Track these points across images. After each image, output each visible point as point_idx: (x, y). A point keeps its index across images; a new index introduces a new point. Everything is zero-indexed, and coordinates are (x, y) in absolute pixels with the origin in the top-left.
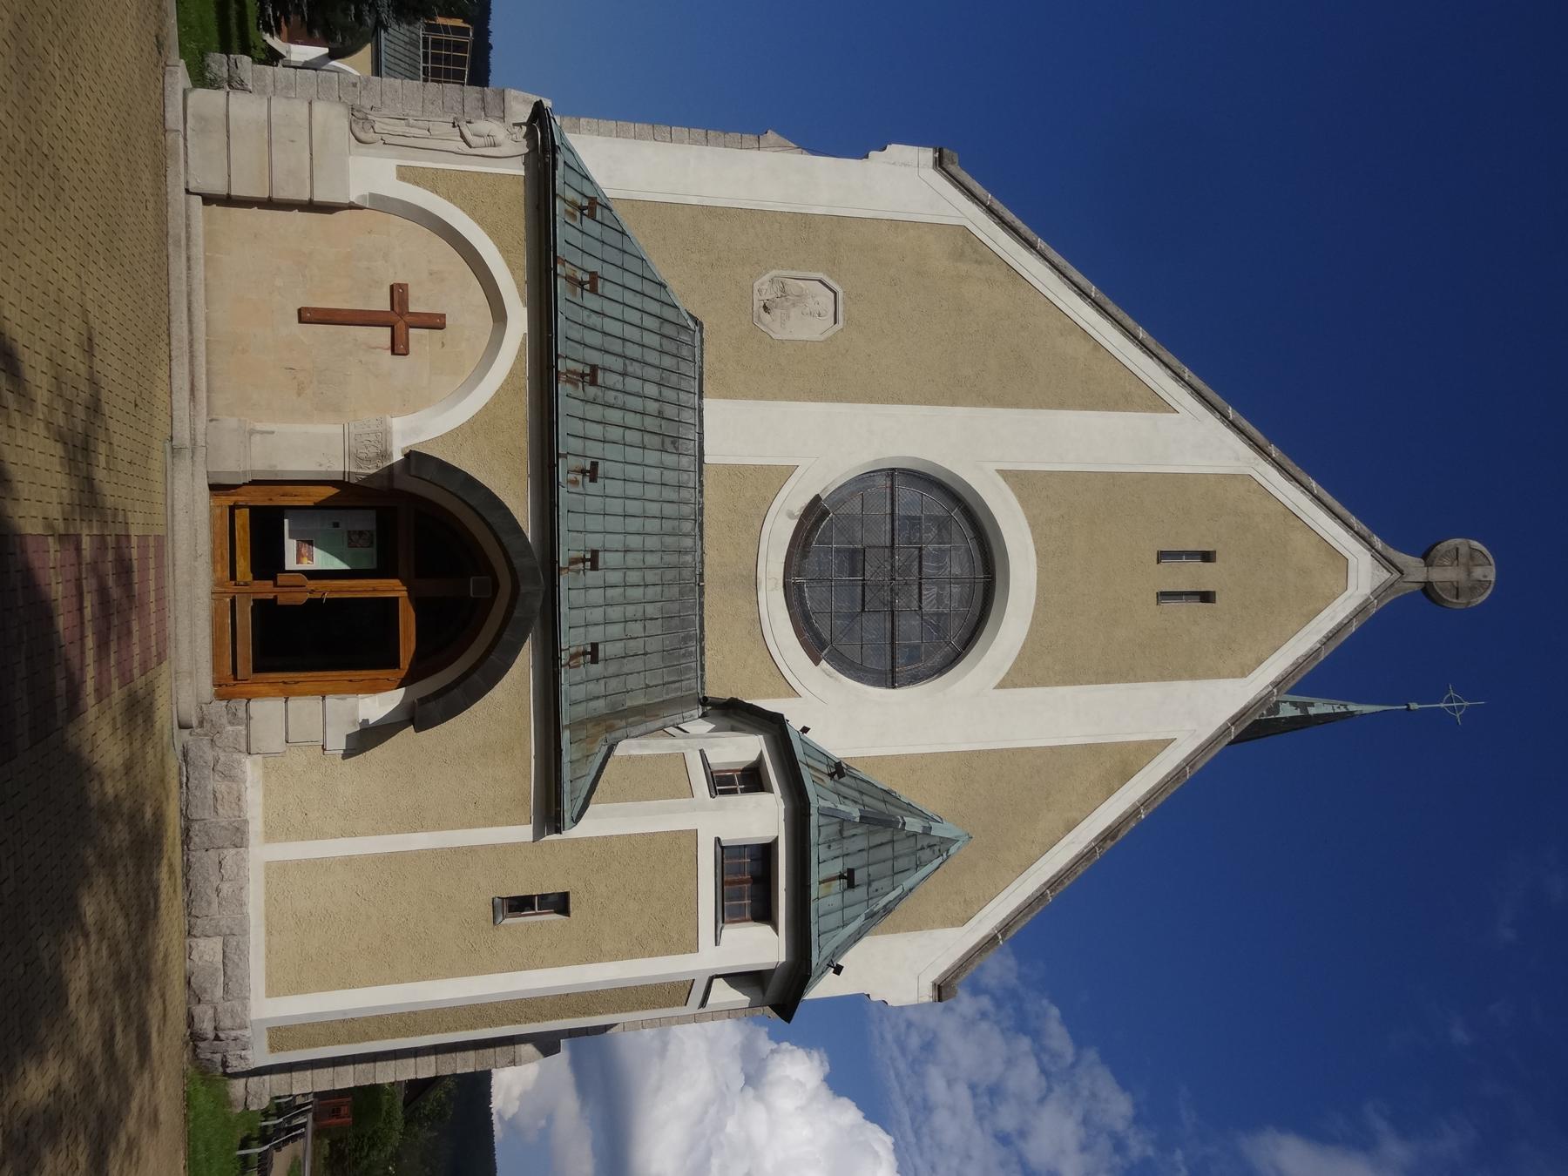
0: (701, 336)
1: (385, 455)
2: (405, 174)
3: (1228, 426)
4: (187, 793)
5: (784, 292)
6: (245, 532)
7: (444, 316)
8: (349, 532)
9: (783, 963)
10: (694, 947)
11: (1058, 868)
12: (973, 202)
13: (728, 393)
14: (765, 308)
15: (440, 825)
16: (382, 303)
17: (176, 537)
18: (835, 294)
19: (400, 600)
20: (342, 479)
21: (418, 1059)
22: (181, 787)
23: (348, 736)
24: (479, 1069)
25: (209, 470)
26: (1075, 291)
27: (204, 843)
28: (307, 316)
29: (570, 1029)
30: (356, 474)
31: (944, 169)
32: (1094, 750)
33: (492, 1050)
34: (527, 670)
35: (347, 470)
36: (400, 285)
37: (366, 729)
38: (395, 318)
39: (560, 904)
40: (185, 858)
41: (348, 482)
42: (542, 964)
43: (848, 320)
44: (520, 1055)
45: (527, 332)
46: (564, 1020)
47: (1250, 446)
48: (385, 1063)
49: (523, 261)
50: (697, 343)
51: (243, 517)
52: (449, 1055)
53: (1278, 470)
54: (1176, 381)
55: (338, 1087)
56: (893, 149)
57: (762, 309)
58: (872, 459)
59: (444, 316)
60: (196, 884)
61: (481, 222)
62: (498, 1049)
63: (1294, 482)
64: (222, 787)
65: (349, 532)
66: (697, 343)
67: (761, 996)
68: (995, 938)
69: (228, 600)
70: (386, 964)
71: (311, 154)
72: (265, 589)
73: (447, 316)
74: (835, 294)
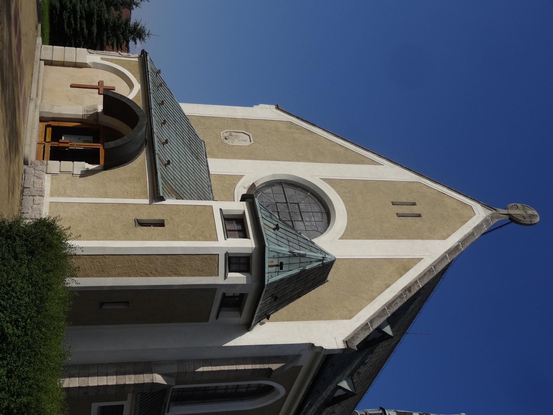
0: (204, 144)
1: (96, 109)
2: (102, 59)
3: (404, 169)
4: (24, 181)
5: (231, 135)
6: (50, 133)
7: (115, 87)
8: (84, 140)
9: (255, 248)
10: (216, 239)
11: (388, 300)
12: (291, 116)
13: (214, 156)
14: (225, 138)
15: (113, 197)
16: (96, 84)
17: (29, 116)
18: (249, 136)
19: (100, 149)
20: (82, 118)
21: (108, 377)
22: (22, 179)
23: (81, 171)
24: (136, 382)
25: (40, 111)
26: (334, 136)
27: (28, 193)
28: (72, 86)
29: (179, 388)
30: (87, 115)
31: (279, 109)
32: (390, 261)
33: (142, 375)
34: (144, 160)
35: (84, 114)
36: (101, 81)
37: (88, 170)
38: (99, 87)
39: (161, 224)
40: (21, 198)
41: (84, 119)
42: (155, 239)
43: (255, 141)
44: (156, 378)
45: (140, 88)
46: (167, 277)
47: (415, 174)
48: (93, 377)
49: (139, 75)
50: (203, 146)
51: (49, 130)
52: (122, 376)
53: (430, 181)
54: (380, 157)
55: (71, 386)
56: (261, 105)
57: (225, 139)
58: (272, 174)
59: (115, 87)
60: (24, 204)
61: (126, 68)
62: (145, 375)
63: (438, 184)
64: (37, 180)
65: (84, 140)
66: (203, 146)
67: (250, 276)
68: (367, 324)
69: (43, 146)
70: (94, 235)
71: (76, 54)
72: (56, 144)
73: (124, 405)
74: (249, 136)
